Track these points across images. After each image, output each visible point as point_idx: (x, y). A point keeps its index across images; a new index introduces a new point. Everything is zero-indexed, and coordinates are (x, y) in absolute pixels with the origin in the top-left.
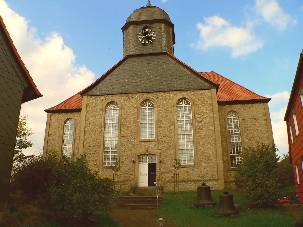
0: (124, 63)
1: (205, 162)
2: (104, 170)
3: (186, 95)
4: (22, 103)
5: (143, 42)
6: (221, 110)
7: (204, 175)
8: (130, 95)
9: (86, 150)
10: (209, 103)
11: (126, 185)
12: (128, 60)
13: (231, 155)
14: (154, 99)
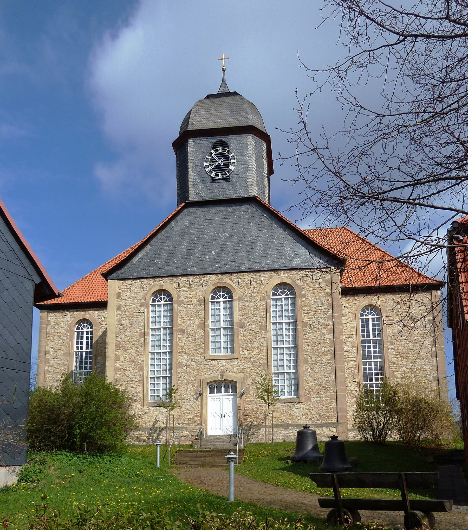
0: (178, 218)
1: (316, 395)
2: (151, 408)
3: (287, 278)
4: (311, 478)
5: (213, 175)
6: (351, 303)
7: (314, 416)
8: (191, 279)
9: (118, 376)
10: (327, 293)
11: (188, 433)
12: (185, 211)
13: (366, 384)
14: (232, 284)
